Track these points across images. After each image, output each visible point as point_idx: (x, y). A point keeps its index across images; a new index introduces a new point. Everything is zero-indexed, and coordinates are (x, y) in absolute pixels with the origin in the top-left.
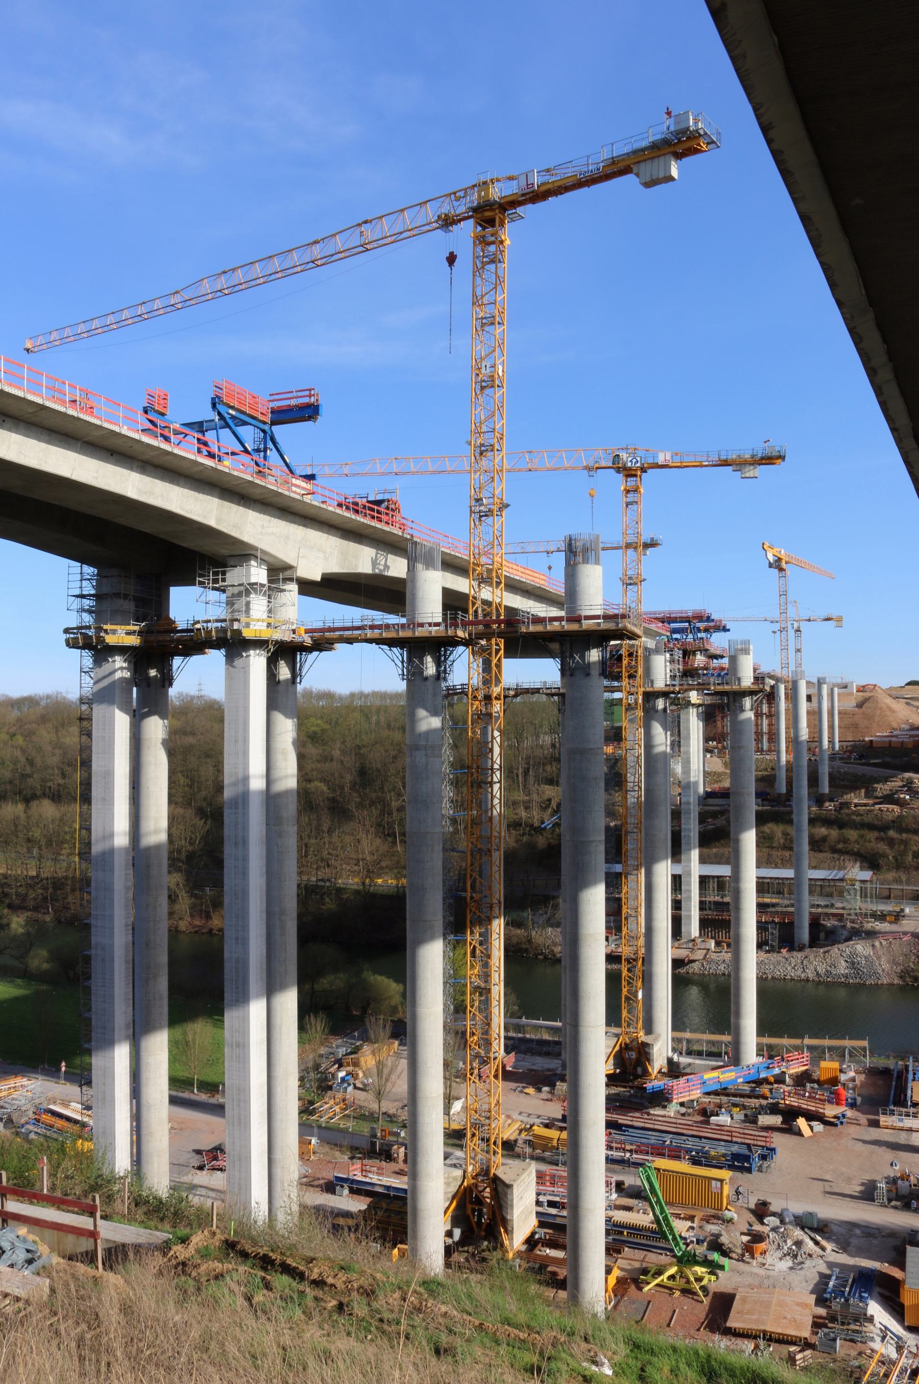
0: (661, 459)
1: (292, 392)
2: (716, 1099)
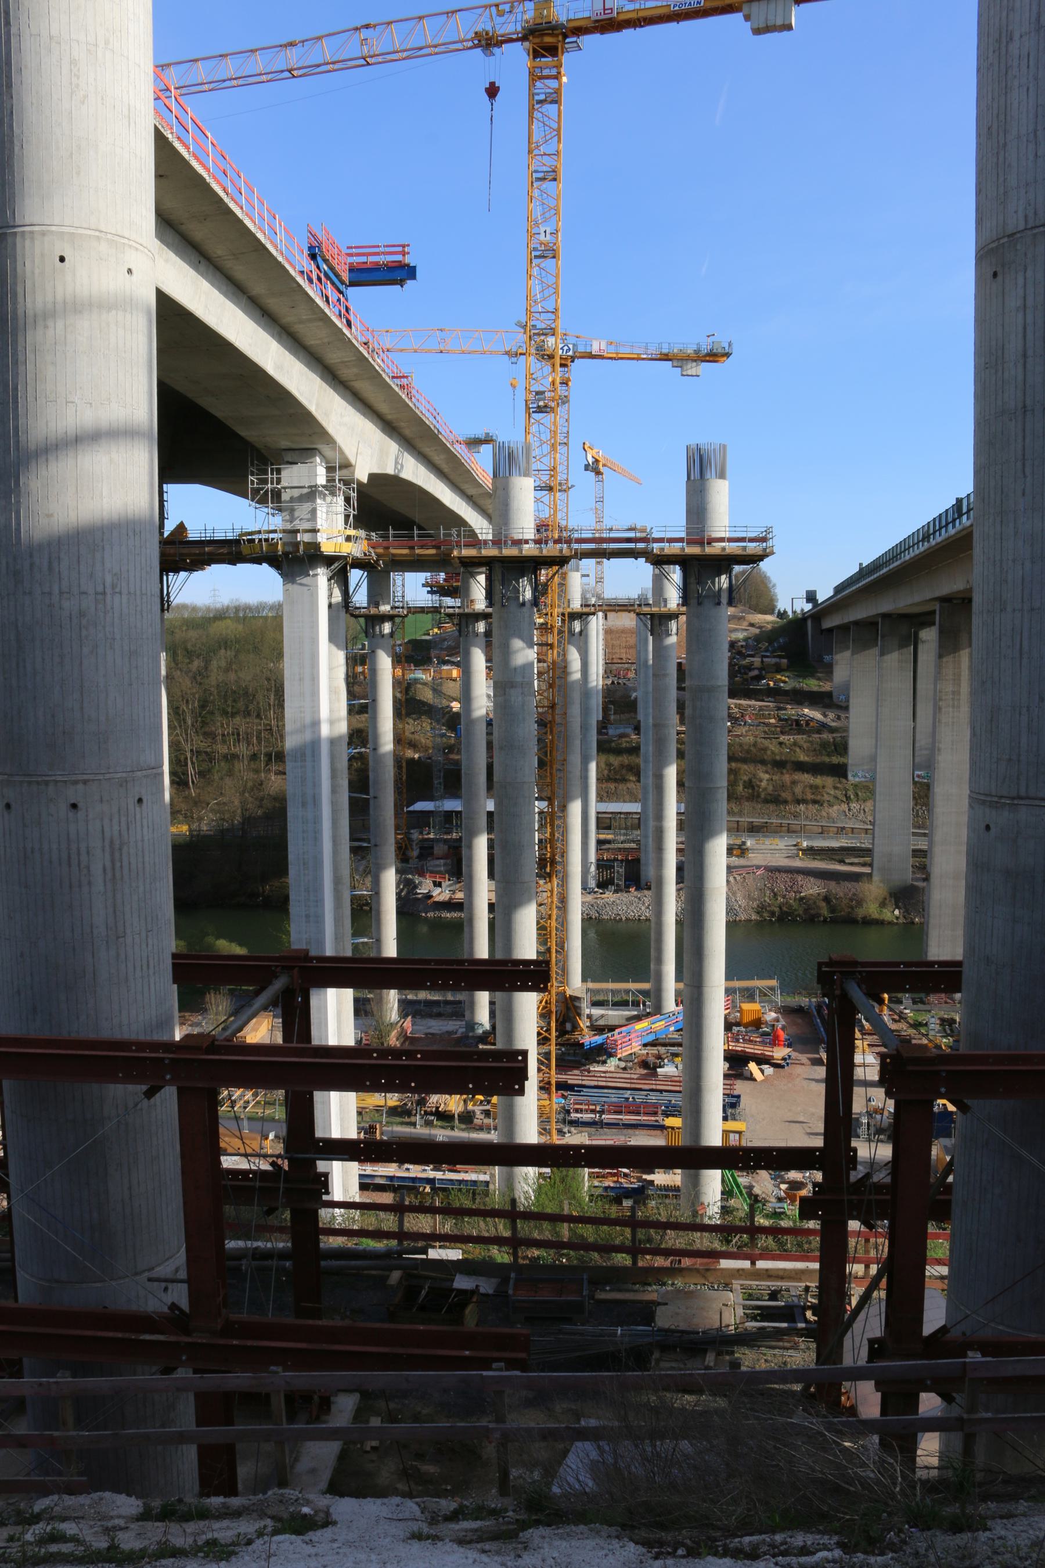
0: (595, 349)
1: (378, 246)
2: (654, 1051)
